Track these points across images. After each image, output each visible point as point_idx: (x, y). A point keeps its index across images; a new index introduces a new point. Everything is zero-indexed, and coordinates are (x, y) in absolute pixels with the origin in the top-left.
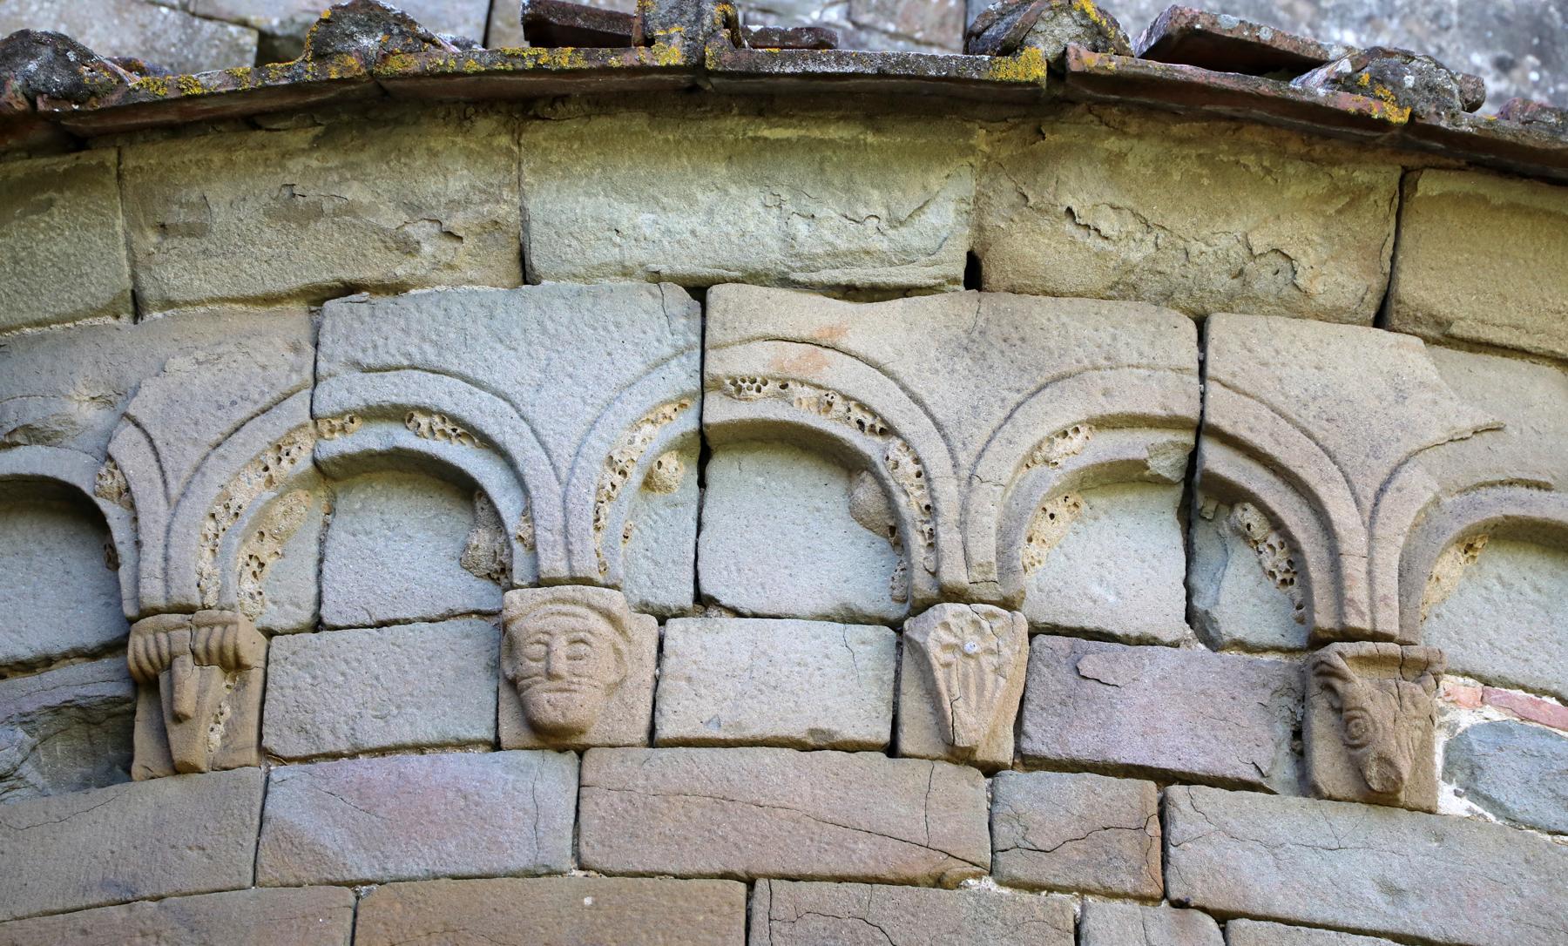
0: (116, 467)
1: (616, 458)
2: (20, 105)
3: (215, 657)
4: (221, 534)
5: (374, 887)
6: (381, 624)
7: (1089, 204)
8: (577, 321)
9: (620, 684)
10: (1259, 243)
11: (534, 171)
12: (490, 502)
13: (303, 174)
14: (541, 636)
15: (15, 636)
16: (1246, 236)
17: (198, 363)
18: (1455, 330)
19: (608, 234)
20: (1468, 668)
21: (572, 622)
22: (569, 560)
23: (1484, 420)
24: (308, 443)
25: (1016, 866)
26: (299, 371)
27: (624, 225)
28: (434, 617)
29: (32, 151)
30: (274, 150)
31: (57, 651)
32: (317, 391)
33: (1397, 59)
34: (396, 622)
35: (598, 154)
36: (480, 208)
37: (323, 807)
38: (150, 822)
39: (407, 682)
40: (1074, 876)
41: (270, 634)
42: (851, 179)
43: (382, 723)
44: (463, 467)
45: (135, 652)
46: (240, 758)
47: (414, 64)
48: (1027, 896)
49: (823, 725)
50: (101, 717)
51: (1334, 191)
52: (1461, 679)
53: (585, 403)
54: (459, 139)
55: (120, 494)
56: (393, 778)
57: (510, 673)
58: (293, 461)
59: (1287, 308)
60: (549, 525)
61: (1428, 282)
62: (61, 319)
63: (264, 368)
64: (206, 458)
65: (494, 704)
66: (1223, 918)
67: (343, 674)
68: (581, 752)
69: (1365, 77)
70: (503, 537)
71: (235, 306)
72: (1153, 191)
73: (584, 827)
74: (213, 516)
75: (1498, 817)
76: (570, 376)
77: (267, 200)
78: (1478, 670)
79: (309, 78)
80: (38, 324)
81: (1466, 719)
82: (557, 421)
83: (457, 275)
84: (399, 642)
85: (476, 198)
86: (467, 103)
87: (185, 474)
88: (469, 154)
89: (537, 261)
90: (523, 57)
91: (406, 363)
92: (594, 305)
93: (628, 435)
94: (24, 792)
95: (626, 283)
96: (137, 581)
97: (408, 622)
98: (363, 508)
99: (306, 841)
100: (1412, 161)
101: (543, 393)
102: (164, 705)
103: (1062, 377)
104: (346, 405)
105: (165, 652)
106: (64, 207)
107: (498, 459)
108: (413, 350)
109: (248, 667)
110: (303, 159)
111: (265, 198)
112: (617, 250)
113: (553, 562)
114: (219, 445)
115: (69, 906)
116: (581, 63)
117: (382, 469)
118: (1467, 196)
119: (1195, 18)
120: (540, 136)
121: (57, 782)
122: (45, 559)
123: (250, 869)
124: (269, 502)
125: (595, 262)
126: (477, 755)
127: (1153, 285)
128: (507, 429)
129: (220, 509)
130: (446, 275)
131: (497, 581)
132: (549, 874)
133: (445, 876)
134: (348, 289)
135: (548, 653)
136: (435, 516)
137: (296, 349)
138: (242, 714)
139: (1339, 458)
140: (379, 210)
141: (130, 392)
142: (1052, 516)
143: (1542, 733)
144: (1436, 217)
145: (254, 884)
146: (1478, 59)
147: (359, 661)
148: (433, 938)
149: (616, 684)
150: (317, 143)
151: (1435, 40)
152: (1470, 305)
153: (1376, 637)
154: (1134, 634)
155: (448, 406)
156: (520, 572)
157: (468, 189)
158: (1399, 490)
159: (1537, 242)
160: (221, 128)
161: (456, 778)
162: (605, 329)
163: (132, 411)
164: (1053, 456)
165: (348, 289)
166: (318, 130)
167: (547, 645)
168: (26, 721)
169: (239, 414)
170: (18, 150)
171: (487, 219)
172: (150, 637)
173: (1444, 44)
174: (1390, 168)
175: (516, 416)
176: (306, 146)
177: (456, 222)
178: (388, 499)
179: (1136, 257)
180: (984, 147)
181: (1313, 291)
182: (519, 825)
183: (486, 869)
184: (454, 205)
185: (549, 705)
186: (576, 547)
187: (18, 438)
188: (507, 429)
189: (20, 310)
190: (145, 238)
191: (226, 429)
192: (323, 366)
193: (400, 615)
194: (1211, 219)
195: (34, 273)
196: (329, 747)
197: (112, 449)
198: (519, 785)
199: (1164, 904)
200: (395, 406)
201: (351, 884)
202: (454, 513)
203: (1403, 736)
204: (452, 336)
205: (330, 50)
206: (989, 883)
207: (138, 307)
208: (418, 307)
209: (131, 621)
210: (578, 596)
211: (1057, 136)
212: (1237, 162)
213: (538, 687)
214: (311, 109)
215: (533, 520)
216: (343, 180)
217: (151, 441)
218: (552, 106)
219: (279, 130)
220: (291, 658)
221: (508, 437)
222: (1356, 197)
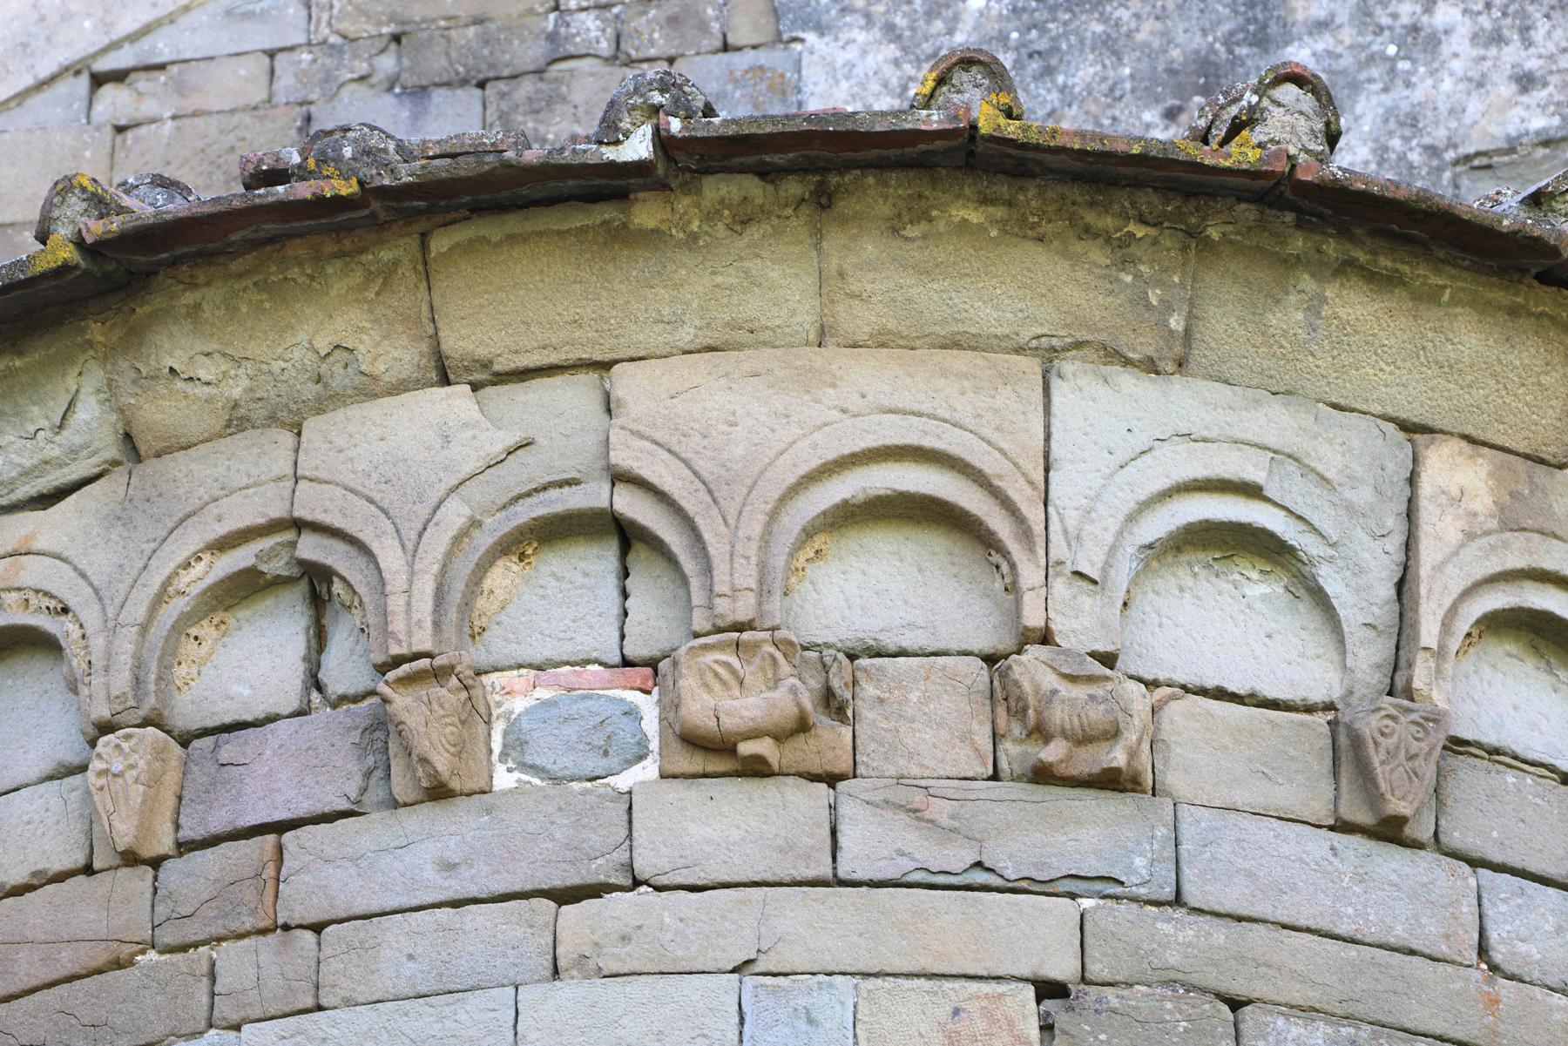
7: (185, 358)
10: (323, 345)
16: (310, 342)
18: (497, 367)
20: (520, 661)
23: (513, 438)
25: (167, 936)
33: (337, 136)
40: (208, 929)
42: (16, 404)
48: (179, 956)
49: (40, 867)
51: (369, 277)
52: (515, 672)
59: (365, 395)
61: (463, 332)
66: (318, 928)
69: (311, 163)
72: (229, 329)
75: (542, 779)
78: (528, 660)
81: (519, 705)
100: (422, 225)
103: (188, 516)
118: (470, 241)
119: (261, 161)
127: (259, 413)
139: (392, 513)
142: (196, 638)
143: (584, 697)
144: (453, 270)
146: (1147, 116)
151: (1109, 113)
152: (502, 340)
153: (417, 656)
154: (262, 716)
158: (437, 524)
159: (537, 263)
164: (182, 587)
173: (1117, 113)
174: (408, 240)
179: (236, 393)
180: (100, 338)
181: (377, 372)
194: (281, 336)
199: (278, 931)
203: (434, 736)
206: (152, 955)
211: (145, 308)
212: (286, 279)
222: (388, 273)
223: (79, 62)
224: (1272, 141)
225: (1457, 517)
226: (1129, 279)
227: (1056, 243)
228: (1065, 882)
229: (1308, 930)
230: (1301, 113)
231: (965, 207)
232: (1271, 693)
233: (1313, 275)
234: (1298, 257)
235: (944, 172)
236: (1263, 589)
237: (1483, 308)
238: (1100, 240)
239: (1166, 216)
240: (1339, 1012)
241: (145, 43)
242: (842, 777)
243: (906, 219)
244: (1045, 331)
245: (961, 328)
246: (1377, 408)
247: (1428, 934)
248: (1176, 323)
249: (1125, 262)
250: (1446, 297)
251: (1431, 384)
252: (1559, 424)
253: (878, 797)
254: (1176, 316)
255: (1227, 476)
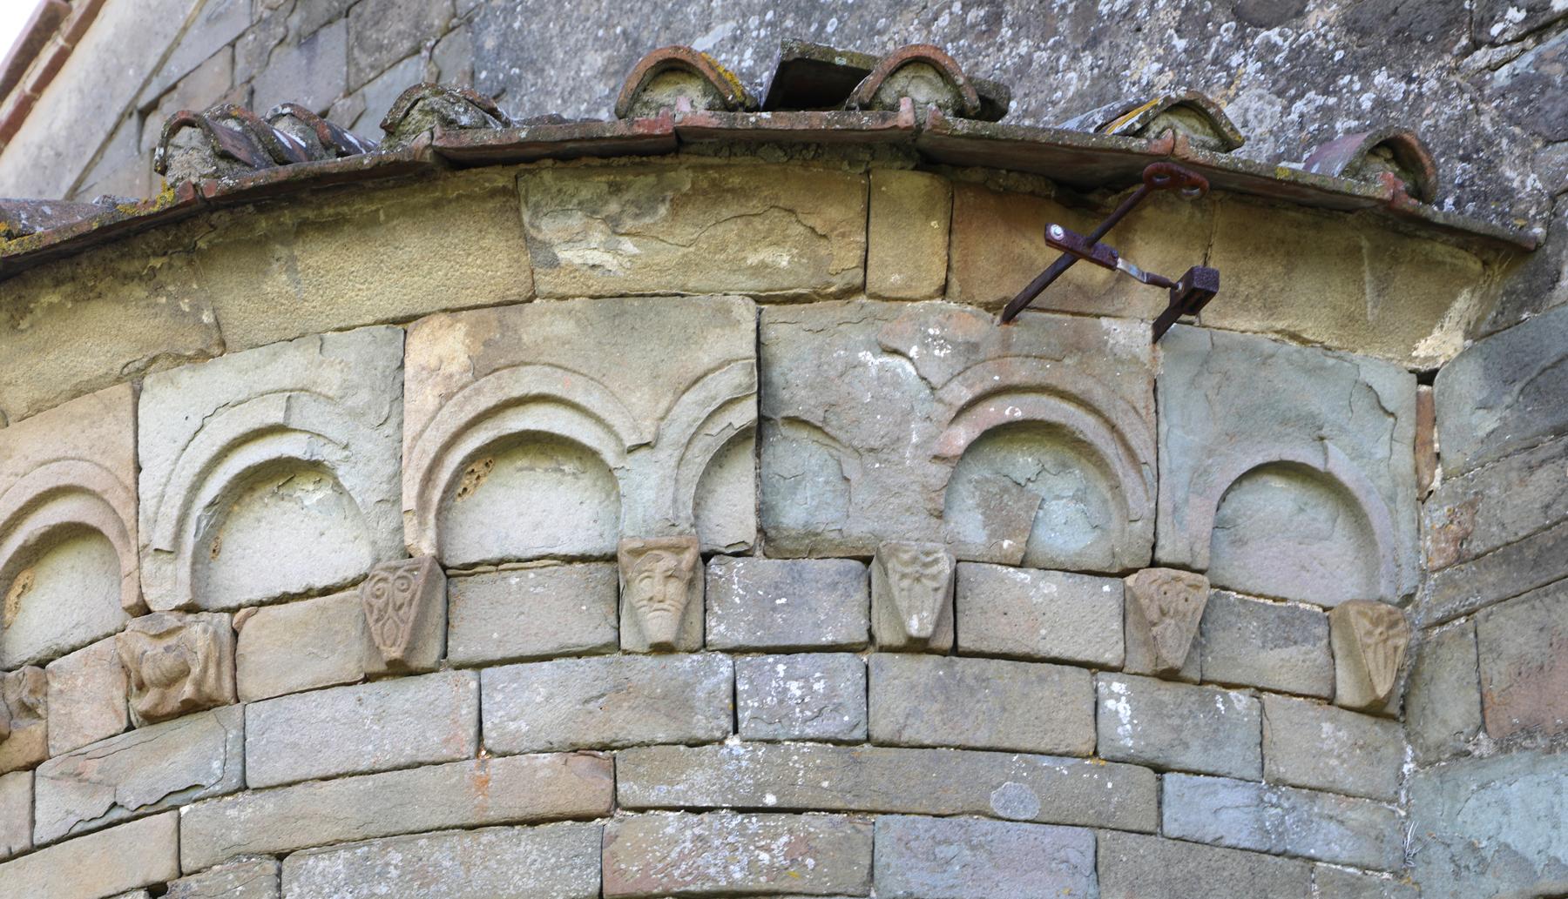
223: (128, 106)
224: (178, 179)
225: (434, 386)
226: (164, 300)
227: (110, 295)
228: (169, 798)
229: (337, 776)
230: (193, 148)
231: (47, 293)
232: (320, 583)
233: (282, 244)
234: (266, 235)
235: (29, 273)
236: (319, 495)
237: (413, 213)
238: (136, 280)
239: (168, 245)
240: (358, 836)
241: (164, 73)
242: (39, 762)
243: (17, 317)
244: (128, 360)
245: (75, 381)
246: (369, 319)
247: (433, 743)
248: (207, 318)
249: (158, 289)
250: (382, 217)
251: (401, 284)
252: (511, 270)
253: (56, 773)
254: (206, 313)
255: (257, 426)
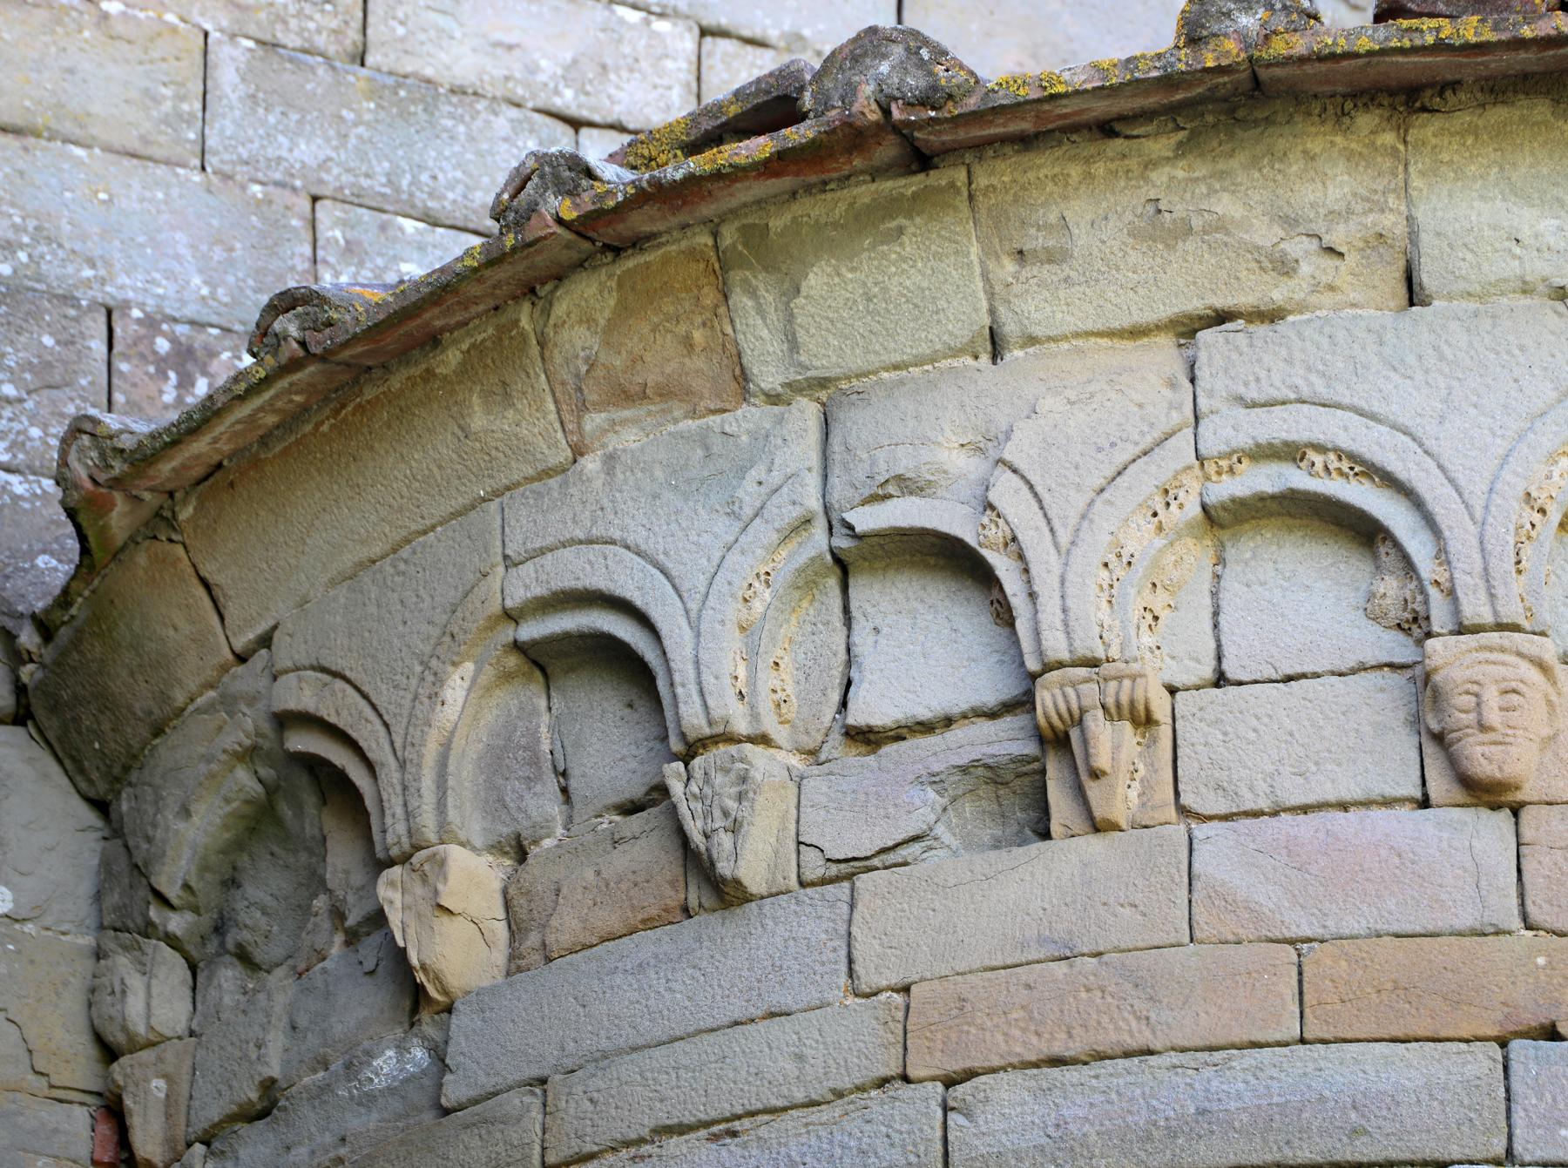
0: (999, 516)
1: (1534, 494)
2: (874, 115)
3: (1126, 711)
4: (1116, 584)
5: (1315, 945)
6: (1289, 679)
8: (1476, 344)
9: (1553, 738)
11: (1422, 173)
12: (1397, 544)
13: (1168, 187)
14: (1469, 686)
15: (910, 696)
17: (1069, 402)
19: (1507, 244)
21: (1501, 671)
22: (1493, 605)
24: (1195, 487)
26: (1179, 408)
27: (1525, 234)
28: (1343, 670)
29: (875, 174)
30: (1135, 160)
31: (956, 710)
32: (1201, 429)
34: (1304, 676)
35: (1495, 150)
36: (1363, 219)
37: (1253, 865)
38: (1077, 880)
39: (1323, 738)
41: (1172, 691)
43: (1301, 780)
44: (1366, 507)
45: (1045, 713)
46: (1159, 816)
47: (1300, 45)
50: (1009, 777)
53: (1494, 434)
54: (1339, 139)
55: (1006, 545)
56: (1321, 835)
57: (1435, 726)
58: (1181, 506)
60: (1467, 568)
62: (919, 362)
63: (1140, 406)
64: (1091, 504)
65: (1418, 760)
67: (1255, 730)
68: (1516, 812)
70: (1415, 583)
71: (1099, 340)
73: (1528, 886)
74: (1106, 565)
76: (1475, 406)
77: (1131, 218)
79: (1183, 68)
80: (896, 367)
82: (1465, 456)
83: (1339, 297)
84: (1310, 696)
85: (1358, 208)
86: (1344, 96)
87: (1073, 520)
88: (1349, 156)
89: (1428, 278)
90: (1422, 31)
91: (1293, 396)
92: (1494, 326)
93: (1543, 470)
94: (940, 853)
95: (1526, 301)
96: (1037, 633)
97: (1316, 675)
98: (1254, 556)
99: (1239, 898)
101: (1447, 425)
102: (1079, 762)
104: (1234, 444)
105: (1075, 707)
106: (914, 235)
107: (1402, 499)
108: (1300, 382)
109: (1157, 723)
110: (1167, 169)
111: (1129, 216)
112: (1517, 263)
113: (1476, 608)
114: (1102, 490)
115: (1009, 961)
116: (1489, 36)
117: (1271, 515)
120: (1429, 131)
121: (970, 844)
122: (930, 617)
123: (1186, 927)
124: (1160, 551)
125: (1493, 278)
126: (1405, 813)
128: (1411, 465)
129: (1112, 558)
130: (1327, 299)
131: (1408, 632)
132: (1497, 933)
133: (1388, 934)
134: (1221, 318)
135: (1478, 705)
136: (1332, 565)
137: (1172, 385)
138: (1156, 771)
140: (1252, 225)
141: (1001, 437)
145: (1192, 940)
147: (1270, 717)
148: (1384, 996)
149: (1550, 738)
150: (1182, 150)
155: (1344, 442)
156: (1440, 617)
157: (1349, 197)
160: (1074, 137)
161: (1387, 835)
162: (1508, 352)
163: (1007, 457)
165: (1221, 318)
166: (1181, 135)
167: (1477, 695)
168: (935, 780)
169: (1122, 457)
170: (862, 172)
171: (1371, 232)
172: (1057, 692)
175: (1419, 451)
176: (1170, 154)
177: (1336, 238)
178: (1280, 547)
182: (1460, 883)
183: (1431, 928)
184: (1334, 216)
185: (1482, 759)
186: (1500, 591)
187: (891, 489)
188: (1411, 465)
189: (877, 353)
190: (1003, 267)
191: (1110, 472)
192: (1203, 402)
193: (1307, 669)
195: (888, 311)
196: (1249, 805)
197: (993, 496)
198: (1455, 843)
200: (1286, 444)
201: (1291, 942)
202: (1352, 561)
204: (1340, 365)
205: (1205, 33)
207: (996, 345)
208: (1299, 334)
209: (1034, 677)
210: (1506, 643)
213: (1471, 739)
214: (1172, 111)
215: (1449, 563)
216: (1212, 191)
217: (1031, 487)
218: (1441, 94)
219: (1138, 137)
220: (1199, 714)
221: (1413, 474)
